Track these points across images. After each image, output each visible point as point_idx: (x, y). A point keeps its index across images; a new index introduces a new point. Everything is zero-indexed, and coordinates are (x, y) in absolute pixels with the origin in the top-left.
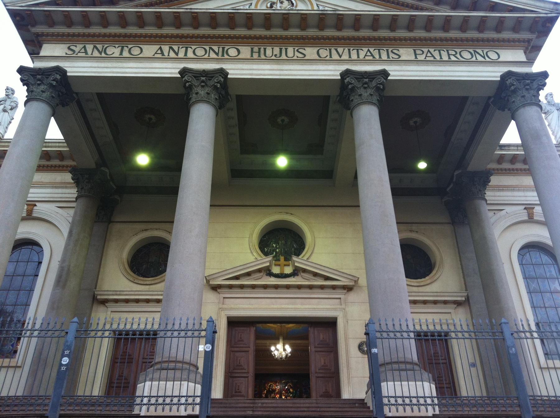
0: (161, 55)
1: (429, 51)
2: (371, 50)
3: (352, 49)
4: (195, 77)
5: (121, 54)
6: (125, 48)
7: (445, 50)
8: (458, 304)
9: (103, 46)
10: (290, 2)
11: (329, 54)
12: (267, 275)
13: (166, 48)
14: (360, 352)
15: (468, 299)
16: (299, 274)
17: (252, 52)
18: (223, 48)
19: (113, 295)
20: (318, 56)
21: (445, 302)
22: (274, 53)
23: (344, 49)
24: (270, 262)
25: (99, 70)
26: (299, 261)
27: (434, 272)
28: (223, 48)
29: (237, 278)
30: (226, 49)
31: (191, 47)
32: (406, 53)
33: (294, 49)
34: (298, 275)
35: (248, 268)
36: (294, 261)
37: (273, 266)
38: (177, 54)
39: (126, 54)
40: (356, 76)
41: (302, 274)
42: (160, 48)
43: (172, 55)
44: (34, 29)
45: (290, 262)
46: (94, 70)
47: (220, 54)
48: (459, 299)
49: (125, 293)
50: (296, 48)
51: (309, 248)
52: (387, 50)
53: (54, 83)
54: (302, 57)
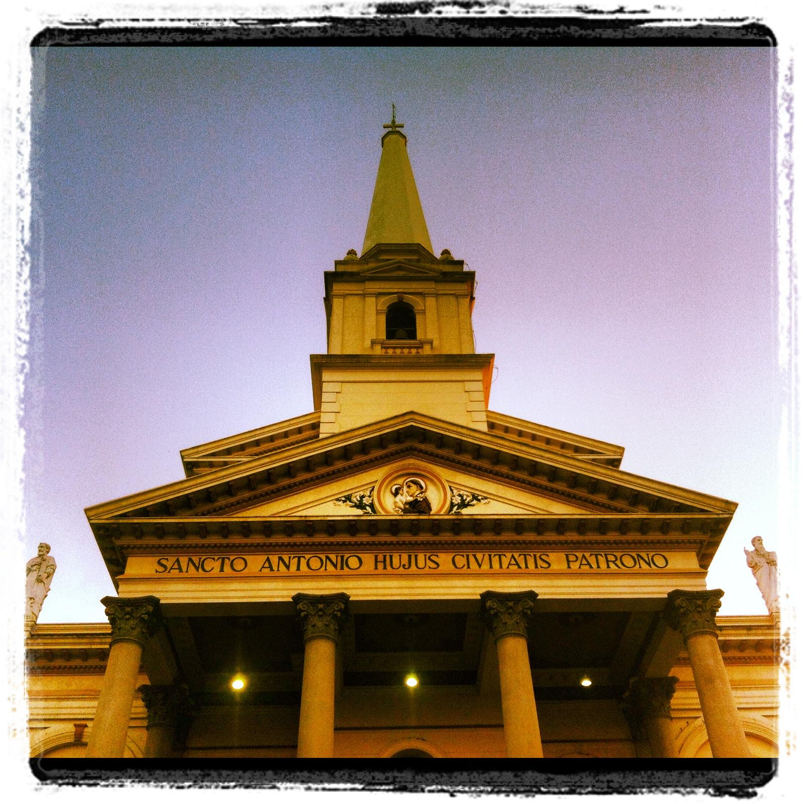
1: (584, 556)
3: (493, 554)
5: (222, 570)
6: (227, 561)
7: (602, 554)
11: (466, 563)
13: (274, 559)
17: (376, 561)
18: (342, 557)
23: (484, 555)
28: (342, 557)
30: (345, 559)
31: (304, 557)
32: (558, 561)
33: (425, 555)
38: (288, 567)
39: (227, 569)
42: (268, 559)
43: (282, 568)
47: (339, 566)
50: (428, 555)
52: (535, 556)
53: (146, 617)
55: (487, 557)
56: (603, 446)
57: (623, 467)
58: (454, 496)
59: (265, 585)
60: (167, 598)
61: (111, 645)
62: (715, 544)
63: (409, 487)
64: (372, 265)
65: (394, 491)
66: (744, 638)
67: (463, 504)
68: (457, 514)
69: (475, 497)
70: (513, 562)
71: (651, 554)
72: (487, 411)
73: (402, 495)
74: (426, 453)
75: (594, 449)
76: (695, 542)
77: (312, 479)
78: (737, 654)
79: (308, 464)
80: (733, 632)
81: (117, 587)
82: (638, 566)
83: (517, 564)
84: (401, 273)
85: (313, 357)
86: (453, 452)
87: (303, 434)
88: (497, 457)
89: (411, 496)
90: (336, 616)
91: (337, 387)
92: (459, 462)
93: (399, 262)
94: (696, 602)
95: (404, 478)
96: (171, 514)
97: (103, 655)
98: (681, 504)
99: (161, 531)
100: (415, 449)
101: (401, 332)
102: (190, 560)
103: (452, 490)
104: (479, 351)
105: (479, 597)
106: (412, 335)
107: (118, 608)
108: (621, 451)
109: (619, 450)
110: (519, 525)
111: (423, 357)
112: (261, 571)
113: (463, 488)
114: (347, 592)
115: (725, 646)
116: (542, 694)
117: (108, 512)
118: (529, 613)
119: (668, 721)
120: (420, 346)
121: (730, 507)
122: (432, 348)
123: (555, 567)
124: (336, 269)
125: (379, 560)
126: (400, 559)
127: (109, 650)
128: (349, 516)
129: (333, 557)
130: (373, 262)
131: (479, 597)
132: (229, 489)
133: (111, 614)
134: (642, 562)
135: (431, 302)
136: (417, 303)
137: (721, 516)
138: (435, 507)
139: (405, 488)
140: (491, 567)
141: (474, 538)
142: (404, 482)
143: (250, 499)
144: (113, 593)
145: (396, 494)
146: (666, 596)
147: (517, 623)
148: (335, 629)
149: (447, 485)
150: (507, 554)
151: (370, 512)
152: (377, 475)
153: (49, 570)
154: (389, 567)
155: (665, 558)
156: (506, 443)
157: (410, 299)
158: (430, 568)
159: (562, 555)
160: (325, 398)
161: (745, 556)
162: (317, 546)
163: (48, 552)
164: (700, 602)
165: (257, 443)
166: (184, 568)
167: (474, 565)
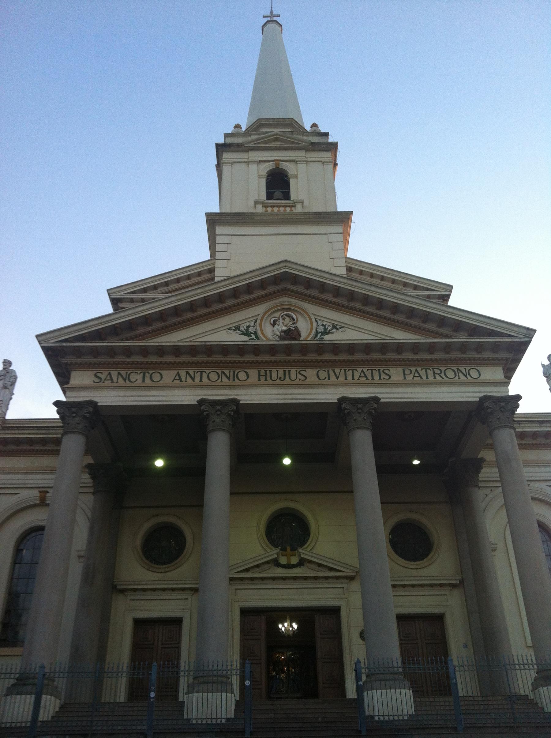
0: (179, 381)
1: (416, 370)
2: (365, 370)
3: (348, 369)
4: (211, 406)
5: (143, 381)
6: (147, 374)
8: (454, 586)
9: (127, 372)
10: (291, 319)
11: (327, 376)
12: (275, 566)
13: (183, 373)
14: (361, 639)
15: (462, 582)
16: (305, 564)
17: (259, 375)
18: (234, 372)
19: (131, 585)
20: (317, 378)
21: (441, 585)
22: (279, 376)
23: (341, 370)
24: (278, 554)
25: (126, 399)
26: (304, 552)
27: (431, 554)
28: (234, 372)
29: (247, 570)
31: (205, 372)
32: (396, 374)
33: (296, 371)
34: (303, 565)
35: (257, 560)
36: (300, 553)
37: (281, 556)
38: (193, 379)
39: (147, 380)
40: (351, 402)
41: (308, 564)
42: (178, 373)
43: (189, 380)
44: (63, 360)
45: (296, 551)
46: (121, 399)
47: (231, 378)
48: (454, 582)
49: (143, 583)
51: (313, 537)
52: (379, 370)
53: (88, 415)
54: (303, 379)
55: (343, 371)
56: (435, 284)
57: (451, 303)
58: (319, 326)
59: (177, 392)
60: (103, 402)
61: (63, 435)
62: (518, 361)
63: (284, 319)
64: (254, 137)
65: (272, 323)
66: (537, 430)
67: (326, 332)
68: (321, 339)
69: (334, 327)
70: (363, 375)
71: (468, 369)
72: (346, 258)
73: (278, 325)
74: (297, 292)
75: (429, 287)
76: (502, 359)
77: (209, 313)
78: (531, 441)
79: (206, 302)
80: (529, 425)
81: (64, 393)
82: (457, 377)
83: (366, 376)
84: (277, 144)
85: (208, 215)
86: (318, 292)
87: (202, 277)
88: (351, 296)
89: (285, 326)
90: (230, 415)
91: (226, 239)
92: (322, 300)
93: (277, 135)
94: (358, 406)
95: (280, 313)
96: (102, 339)
97: (58, 442)
98: (492, 330)
99: (95, 352)
100: (289, 290)
101: (278, 193)
102: (119, 373)
103: (316, 321)
104: (340, 209)
105: (336, 401)
106: (287, 196)
107: (210, 407)
108: (450, 288)
109: (448, 288)
110: (367, 348)
111: (295, 214)
112: (173, 382)
113: (325, 320)
114: (238, 398)
115: (521, 436)
116: (381, 470)
117: (55, 337)
118: (374, 412)
119: (477, 489)
120: (293, 205)
121: (530, 333)
122: (303, 207)
123: (394, 378)
124: (225, 141)
125: (261, 374)
126: (277, 373)
127: (62, 437)
128: (238, 341)
129: (227, 372)
130: (254, 134)
131: (336, 401)
132: (146, 320)
133: (62, 413)
134: (461, 374)
135: (302, 167)
136: (290, 168)
137: (523, 340)
138: (304, 335)
139: (281, 320)
140: (346, 379)
141: (333, 358)
142: (280, 315)
143: (162, 328)
144: (62, 398)
145: (274, 324)
146: (478, 399)
147: (365, 419)
148: (230, 424)
149: (313, 318)
150: (358, 369)
151: (255, 338)
152: (259, 310)
153: (12, 380)
154: (269, 379)
155: (478, 371)
156: (360, 285)
157: (284, 166)
158: (300, 380)
159: (400, 370)
160: (218, 248)
161: (542, 369)
162: (214, 363)
163: (10, 366)
164: (503, 404)
165: (167, 284)
166: (115, 380)
167: (333, 378)
